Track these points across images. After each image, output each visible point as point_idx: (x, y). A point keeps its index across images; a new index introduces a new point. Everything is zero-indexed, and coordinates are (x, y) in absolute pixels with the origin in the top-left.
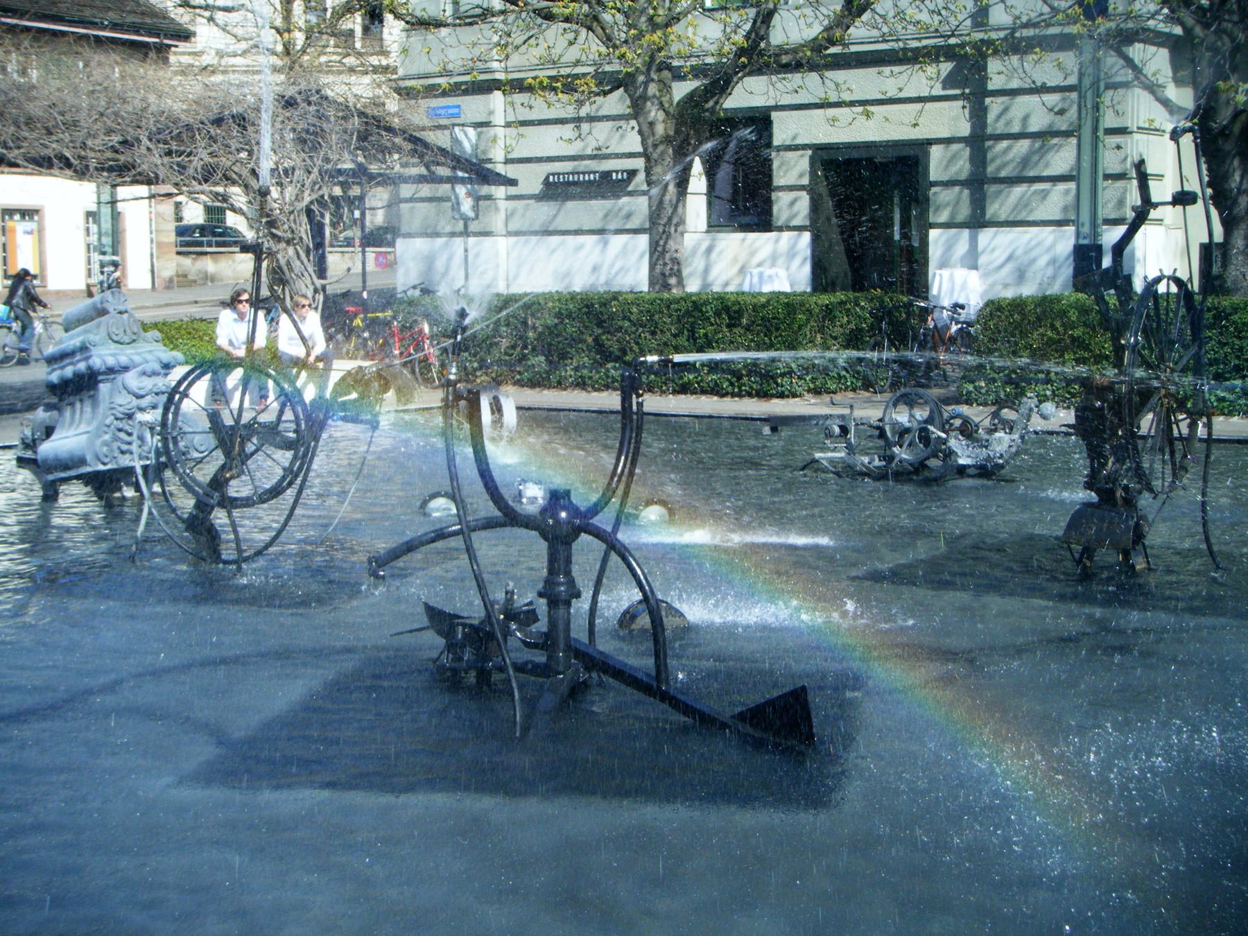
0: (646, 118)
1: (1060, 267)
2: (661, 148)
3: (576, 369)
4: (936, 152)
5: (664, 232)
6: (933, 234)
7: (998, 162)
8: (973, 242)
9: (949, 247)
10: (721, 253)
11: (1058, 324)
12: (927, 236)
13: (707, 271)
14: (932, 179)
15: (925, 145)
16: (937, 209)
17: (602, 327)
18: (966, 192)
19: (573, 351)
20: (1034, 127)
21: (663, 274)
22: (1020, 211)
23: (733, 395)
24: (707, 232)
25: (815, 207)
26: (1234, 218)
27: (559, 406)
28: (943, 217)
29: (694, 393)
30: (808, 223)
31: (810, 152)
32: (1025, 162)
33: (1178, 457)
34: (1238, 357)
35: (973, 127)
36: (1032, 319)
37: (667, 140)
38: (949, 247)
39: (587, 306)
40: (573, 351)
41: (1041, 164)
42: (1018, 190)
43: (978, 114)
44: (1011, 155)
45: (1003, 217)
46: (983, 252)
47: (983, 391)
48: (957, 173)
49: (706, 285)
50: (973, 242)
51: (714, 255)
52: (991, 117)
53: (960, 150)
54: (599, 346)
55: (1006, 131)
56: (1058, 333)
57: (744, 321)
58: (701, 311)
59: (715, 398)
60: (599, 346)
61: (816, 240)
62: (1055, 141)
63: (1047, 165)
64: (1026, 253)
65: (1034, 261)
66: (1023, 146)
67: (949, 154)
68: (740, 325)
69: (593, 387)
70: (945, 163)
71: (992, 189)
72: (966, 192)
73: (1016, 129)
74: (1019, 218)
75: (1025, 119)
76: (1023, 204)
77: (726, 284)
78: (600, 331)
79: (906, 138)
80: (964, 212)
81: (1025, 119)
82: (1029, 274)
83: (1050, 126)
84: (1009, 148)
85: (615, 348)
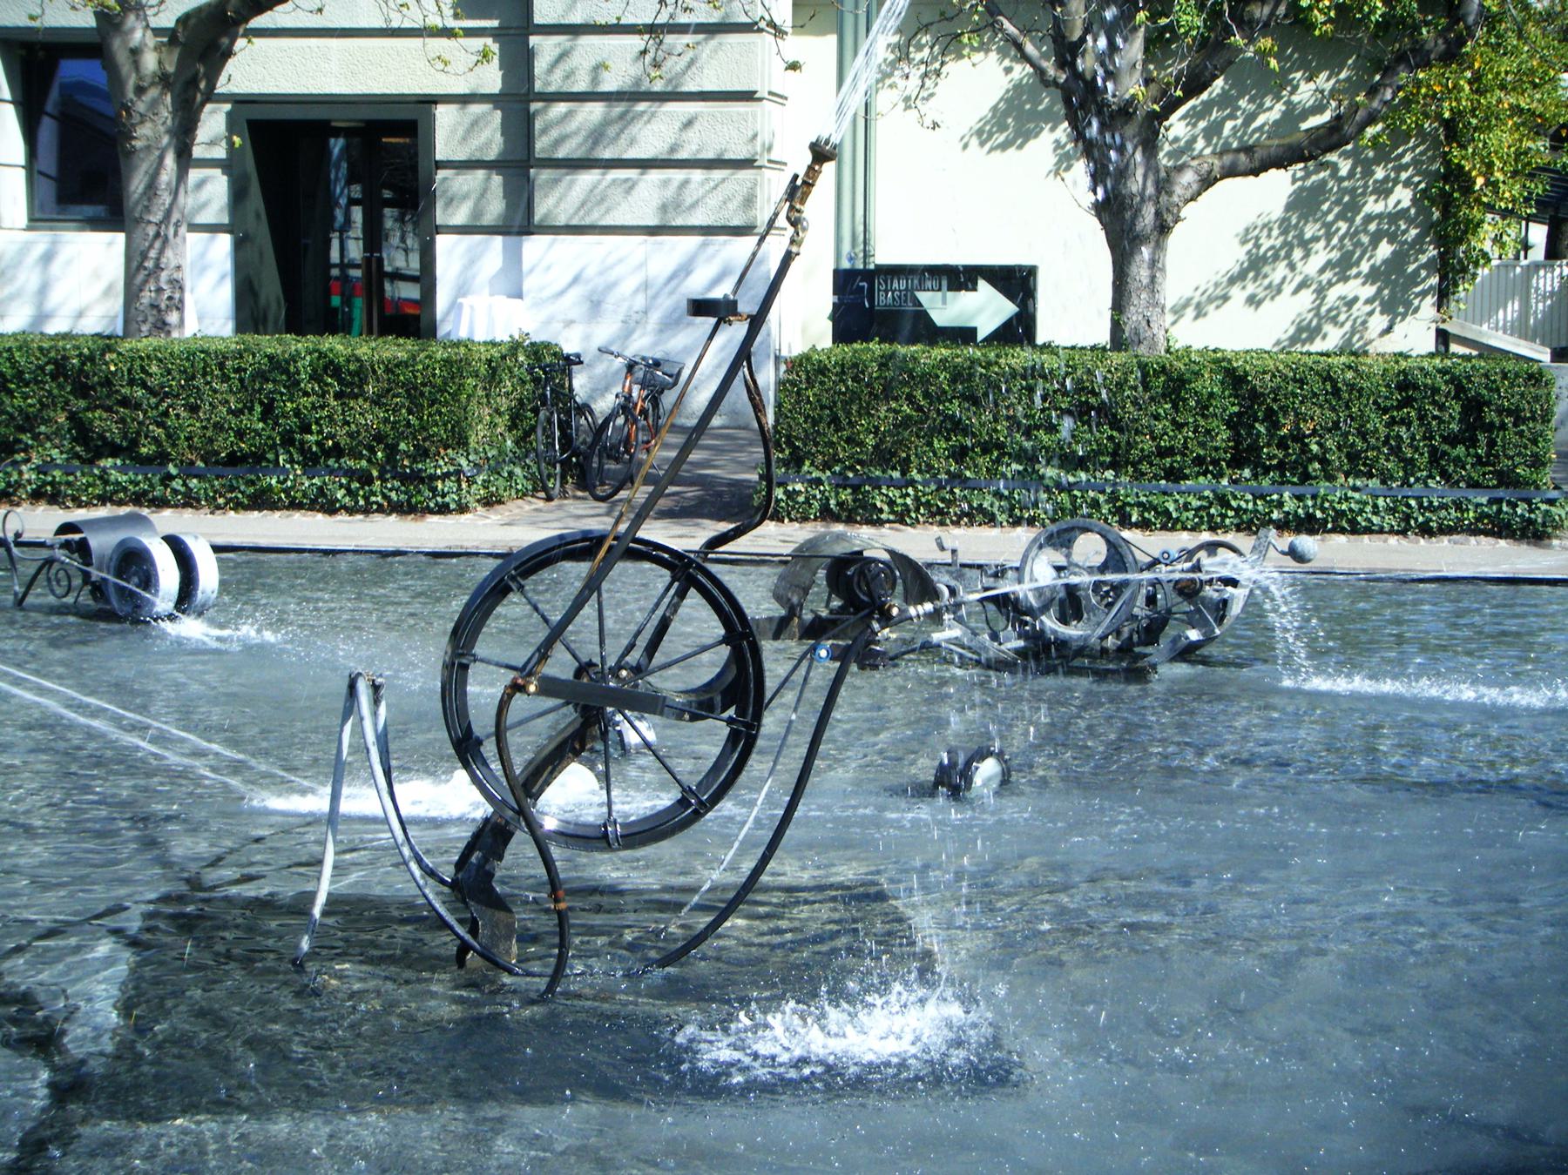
0: (125, 42)
1: (655, 297)
2: (153, 93)
3: (39, 470)
4: (444, 116)
5: (157, 235)
6: (443, 242)
7: (554, 134)
8: (513, 259)
9: (472, 261)
10: (69, 263)
11: (918, 394)
12: (432, 244)
13: (43, 290)
14: (438, 157)
15: (430, 101)
16: (450, 202)
17: (85, 396)
18: (497, 180)
19: (26, 438)
20: (609, 84)
21: (154, 306)
22: (588, 213)
23: (351, 511)
24: (29, 229)
25: (238, 195)
26: (1138, 236)
27: (263, 542)
28: (460, 216)
29: (274, 506)
30: (226, 220)
31: (228, 107)
32: (597, 135)
33: (1544, 622)
34: (1202, 445)
35: (505, 79)
36: (878, 388)
37: (164, 80)
38: (472, 261)
39: (55, 362)
40: (26, 438)
41: (623, 141)
42: (587, 178)
43: (518, 62)
44: (573, 125)
45: (561, 220)
46: (531, 271)
47: (801, 499)
48: (480, 149)
49: (42, 317)
50: (513, 259)
51: (56, 267)
52: (540, 65)
53: (484, 115)
54: (81, 431)
55: (565, 89)
56: (919, 409)
57: (370, 389)
58: (286, 372)
59: (320, 516)
60: (81, 431)
61: (239, 246)
62: (642, 106)
63: (632, 142)
64: (601, 273)
65: (611, 286)
66: (593, 112)
67: (467, 121)
68: (362, 394)
69: (75, 499)
70: (460, 132)
71: (542, 176)
72: (497, 180)
73: (581, 85)
74: (587, 221)
75: (599, 67)
76: (594, 198)
77: (80, 315)
78: (82, 404)
79: (305, 91)
80: (495, 208)
81: (599, 67)
82: (608, 306)
83: (638, 82)
84: (569, 115)
85: (114, 431)
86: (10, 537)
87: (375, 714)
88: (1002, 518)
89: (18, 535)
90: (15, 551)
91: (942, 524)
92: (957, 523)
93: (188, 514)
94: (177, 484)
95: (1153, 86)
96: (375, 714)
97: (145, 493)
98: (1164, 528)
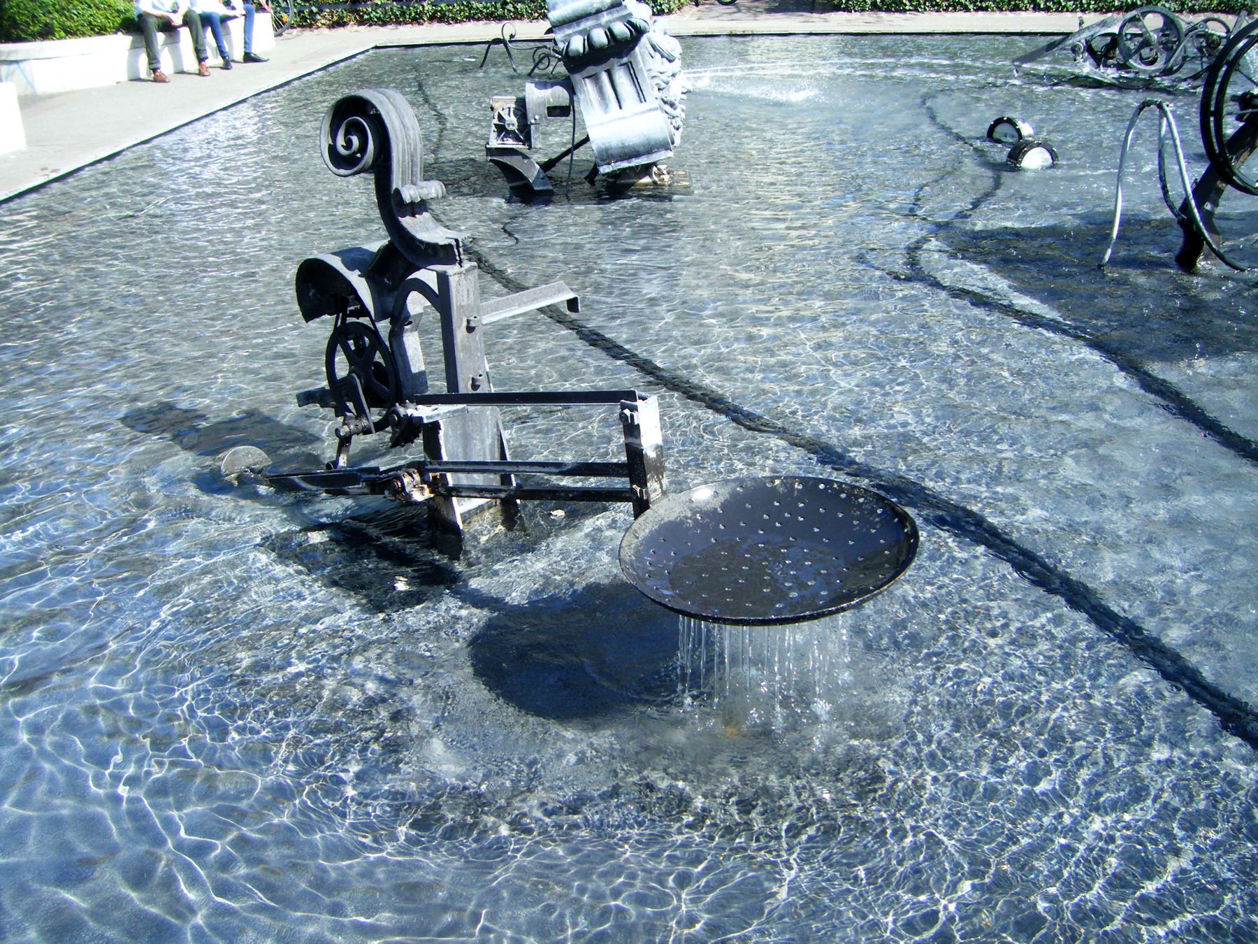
31: (479, 616)
86: (507, 38)
87: (1169, 125)
88: (971, 7)
89: (512, 36)
90: (510, 45)
91: (938, 11)
92: (946, 10)
93: (517, 22)
94: (510, 7)
95: (394, 691)
96: (1169, 125)
97: (493, 13)
98: (1057, 10)
